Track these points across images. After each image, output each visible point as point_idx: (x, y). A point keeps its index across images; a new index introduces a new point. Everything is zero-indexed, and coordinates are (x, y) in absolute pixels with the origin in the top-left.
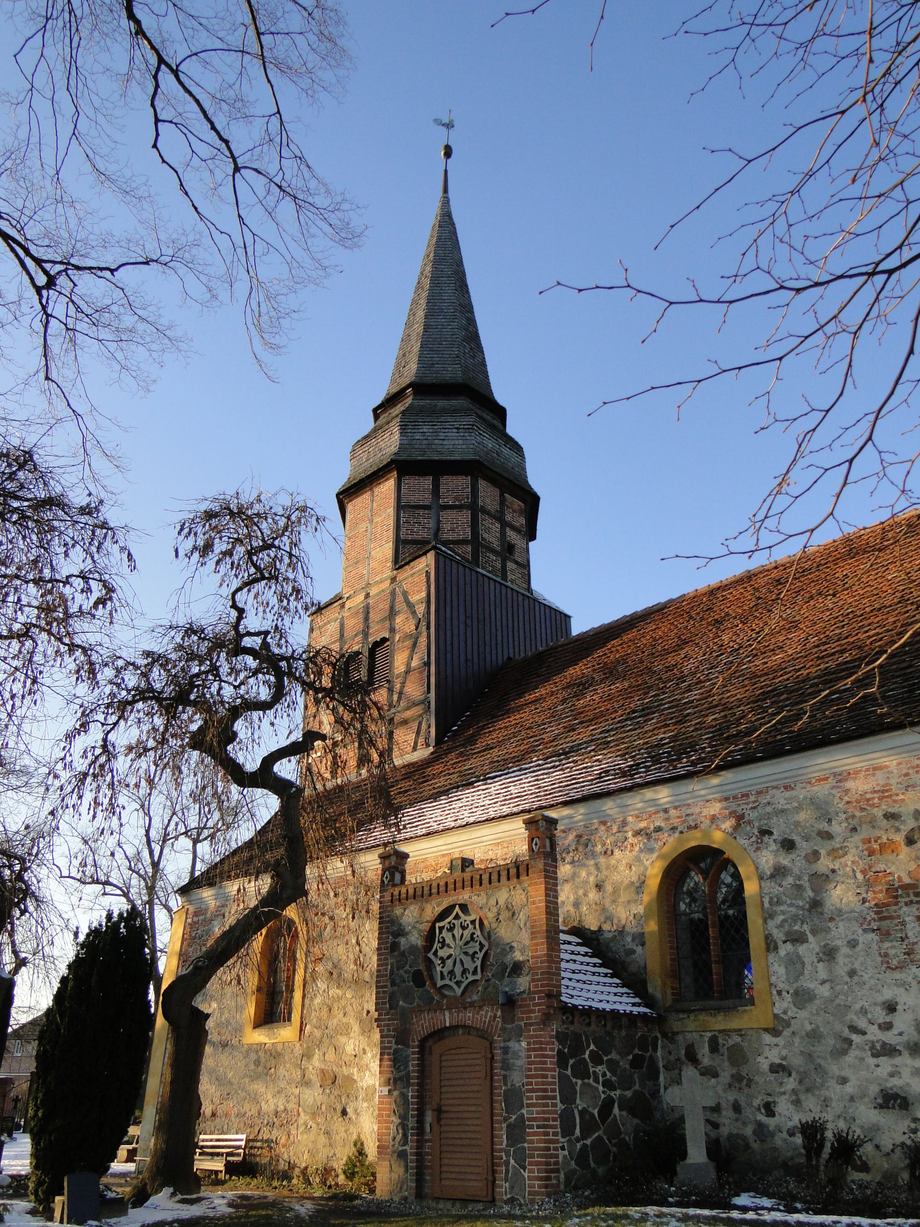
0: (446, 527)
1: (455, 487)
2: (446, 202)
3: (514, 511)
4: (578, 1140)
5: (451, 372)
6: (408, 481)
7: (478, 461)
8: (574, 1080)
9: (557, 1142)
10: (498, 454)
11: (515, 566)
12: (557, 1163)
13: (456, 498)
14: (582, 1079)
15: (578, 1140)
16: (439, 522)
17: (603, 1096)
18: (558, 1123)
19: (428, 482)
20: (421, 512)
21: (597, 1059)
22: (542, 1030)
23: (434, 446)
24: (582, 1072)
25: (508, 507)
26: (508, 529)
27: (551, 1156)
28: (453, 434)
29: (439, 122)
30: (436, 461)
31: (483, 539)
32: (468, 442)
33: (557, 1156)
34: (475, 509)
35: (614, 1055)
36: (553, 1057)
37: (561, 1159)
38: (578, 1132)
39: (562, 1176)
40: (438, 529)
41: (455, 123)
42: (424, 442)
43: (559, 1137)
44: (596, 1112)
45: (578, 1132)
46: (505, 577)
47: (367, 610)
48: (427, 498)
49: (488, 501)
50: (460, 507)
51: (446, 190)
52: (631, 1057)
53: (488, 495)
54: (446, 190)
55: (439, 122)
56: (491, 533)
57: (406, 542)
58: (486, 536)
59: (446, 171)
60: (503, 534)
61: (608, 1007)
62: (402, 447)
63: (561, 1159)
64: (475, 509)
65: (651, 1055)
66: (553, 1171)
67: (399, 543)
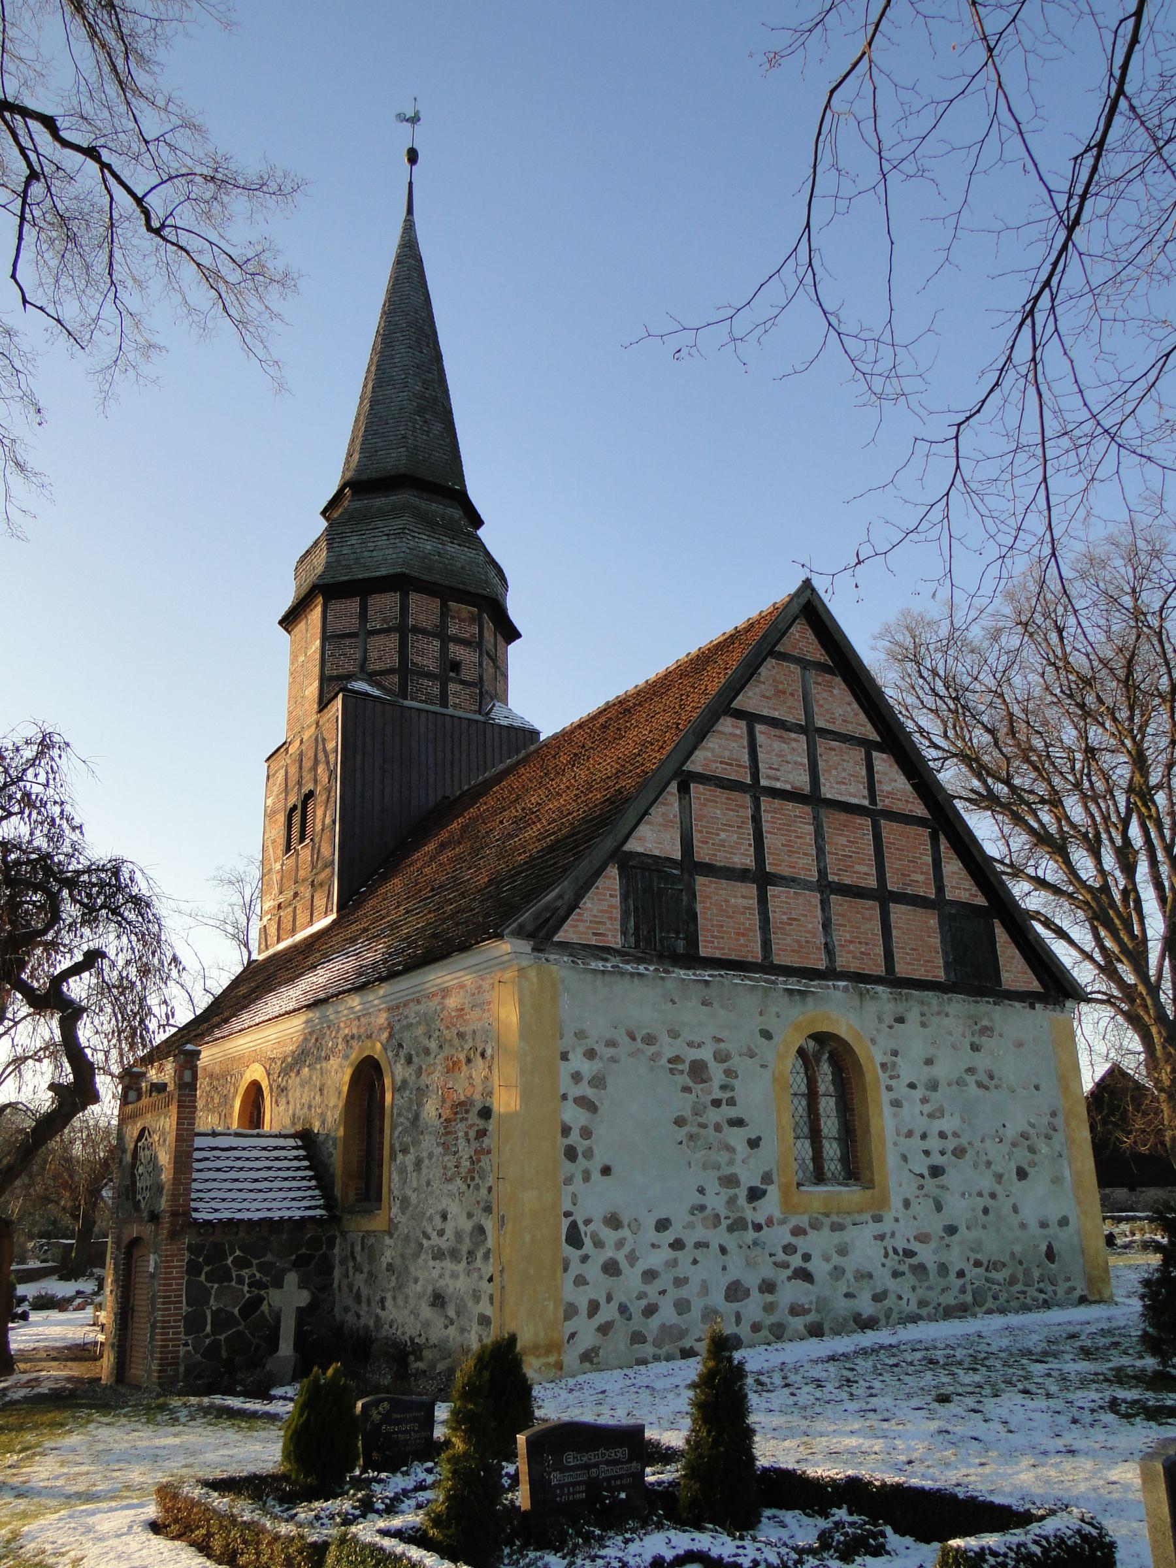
0: (373, 655)
1: (385, 605)
2: (409, 226)
3: (461, 620)
4: (207, 1336)
5: (394, 460)
6: (334, 605)
7: (403, 575)
8: (209, 1285)
9: (180, 1340)
10: (439, 554)
11: (459, 687)
12: (178, 1357)
13: (384, 620)
14: (220, 1282)
15: (207, 1336)
16: (366, 651)
17: (248, 1295)
18: (182, 1324)
19: (354, 605)
20: (347, 641)
21: (241, 1263)
22: (170, 1244)
23: (362, 561)
24: (222, 1275)
25: (453, 618)
26: (451, 645)
27: (170, 1352)
28: (383, 542)
29: (402, 118)
30: (360, 580)
31: (414, 664)
32: (398, 550)
33: (178, 1352)
34: (403, 630)
35: (269, 1257)
36: (182, 1267)
37: (181, 1354)
38: (208, 1328)
39: (182, 1369)
40: (365, 659)
41: (421, 116)
42: (352, 556)
43: (182, 1336)
44: (236, 1311)
45: (208, 1328)
46: (444, 704)
47: (301, 755)
48: (353, 624)
49: (422, 617)
50: (387, 631)
51: (410, 211)
52: (294, 1257)
53: (423, 610)
54: (410, 211)
55: (402, 118)
56: (427, 654)
57: (332, 679)
58: (418, 660)
59: (411, 184)
60: (444, 650)
61: (256, 1216)
62: (328, 566)
63: (181, 1354)
64: (403, 630)
65: (324, 1254)
66: (170, 1364)
67: (324, 680)
